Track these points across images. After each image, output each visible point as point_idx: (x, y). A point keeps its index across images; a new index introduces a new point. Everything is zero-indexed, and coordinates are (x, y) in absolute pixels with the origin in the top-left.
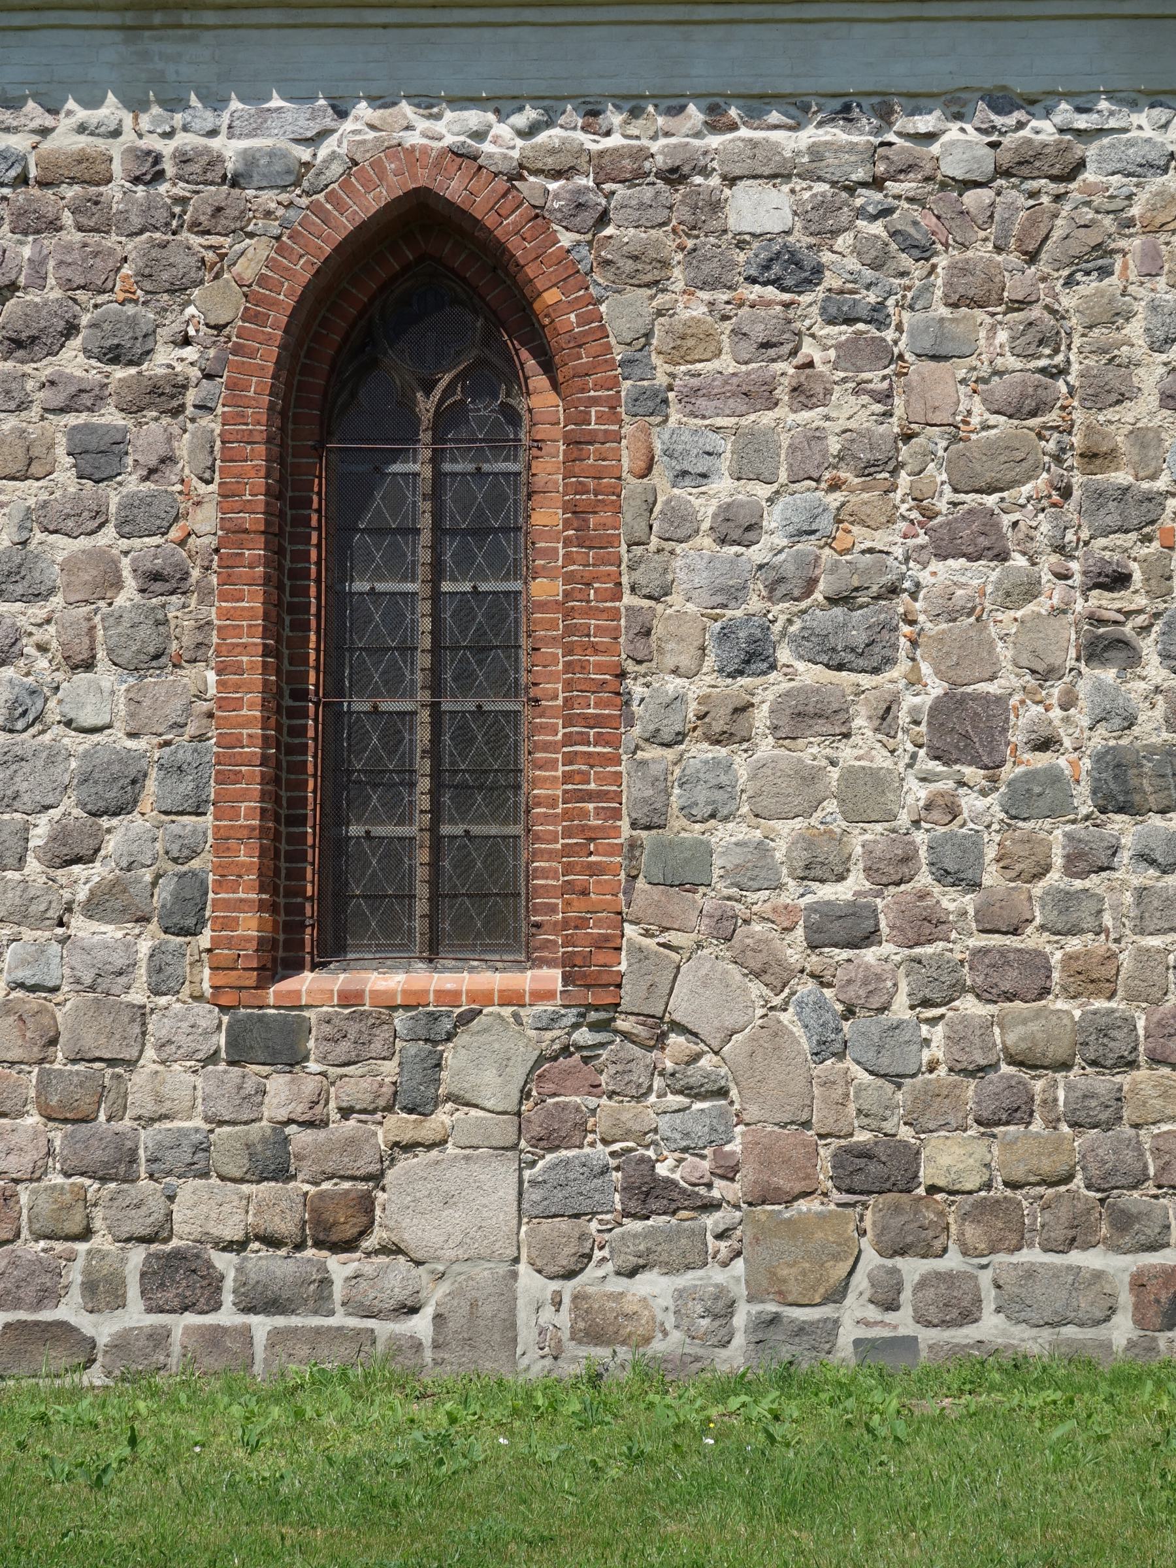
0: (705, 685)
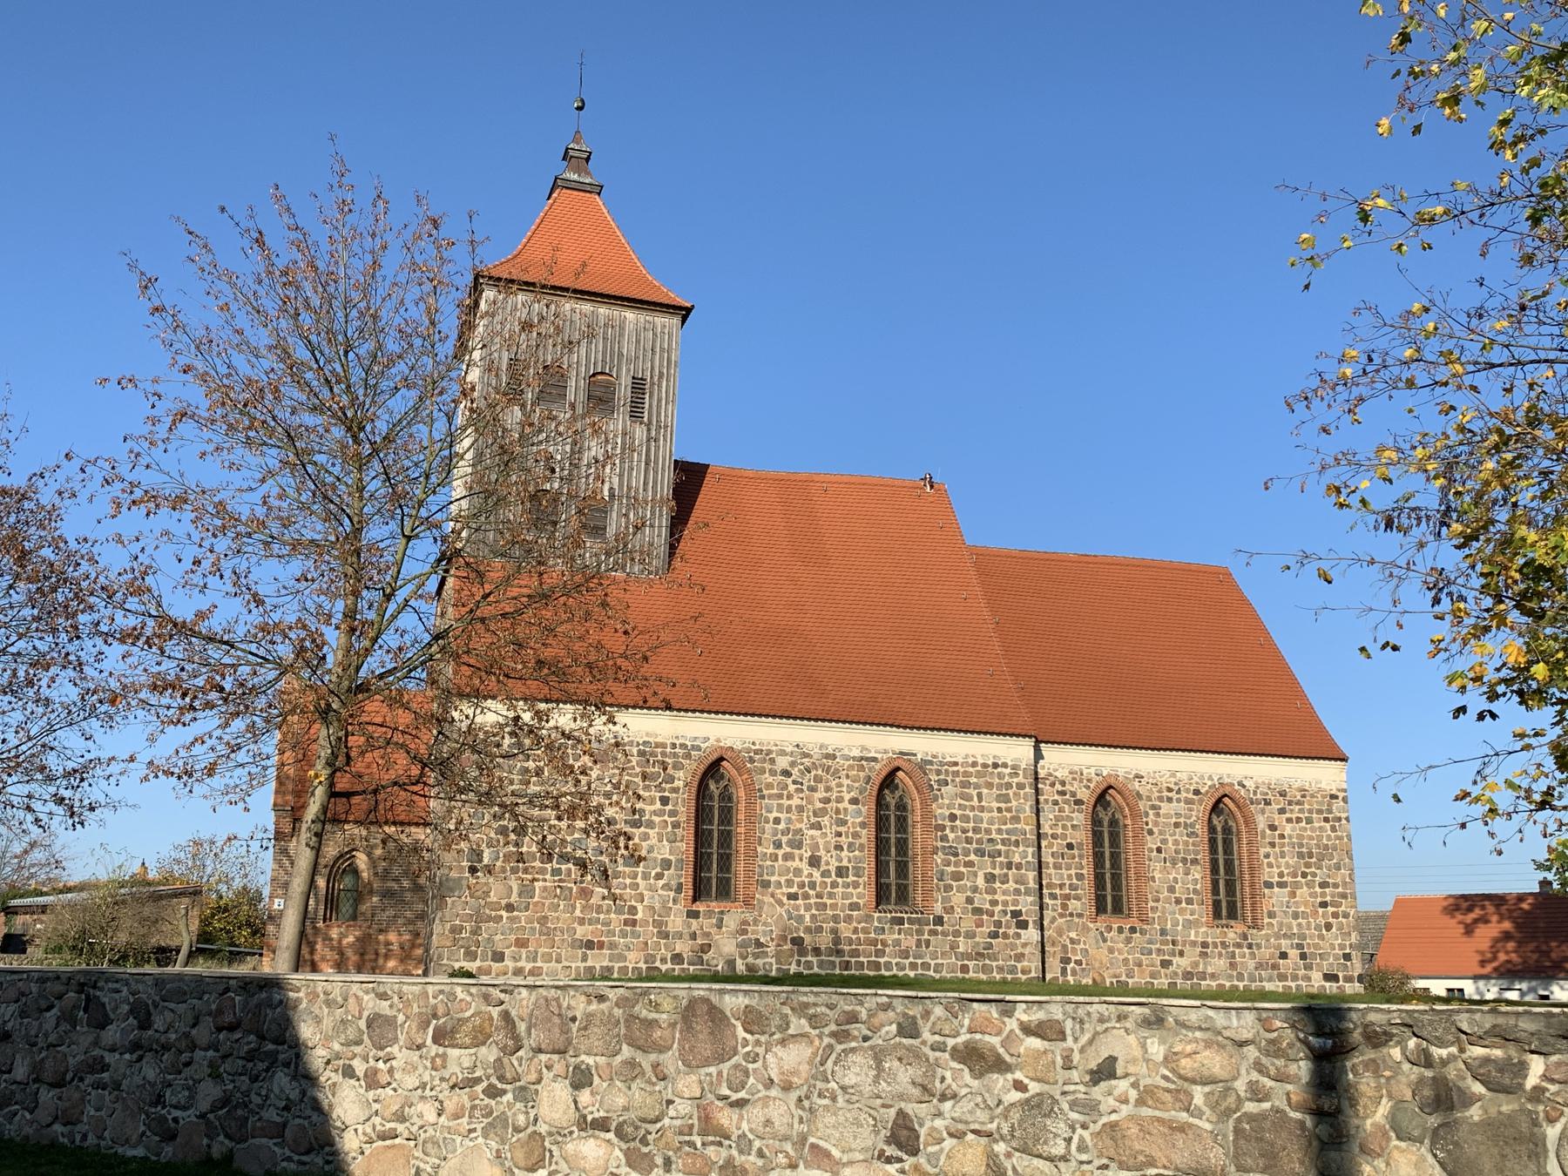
0: (771, 850)
